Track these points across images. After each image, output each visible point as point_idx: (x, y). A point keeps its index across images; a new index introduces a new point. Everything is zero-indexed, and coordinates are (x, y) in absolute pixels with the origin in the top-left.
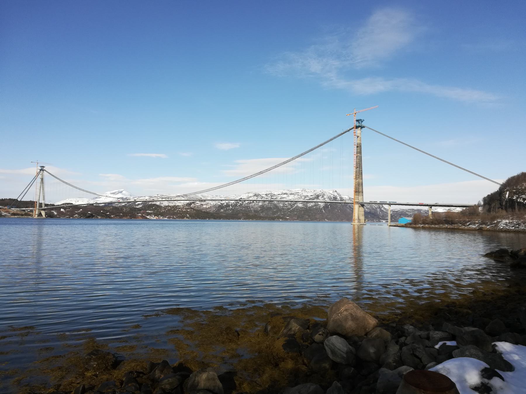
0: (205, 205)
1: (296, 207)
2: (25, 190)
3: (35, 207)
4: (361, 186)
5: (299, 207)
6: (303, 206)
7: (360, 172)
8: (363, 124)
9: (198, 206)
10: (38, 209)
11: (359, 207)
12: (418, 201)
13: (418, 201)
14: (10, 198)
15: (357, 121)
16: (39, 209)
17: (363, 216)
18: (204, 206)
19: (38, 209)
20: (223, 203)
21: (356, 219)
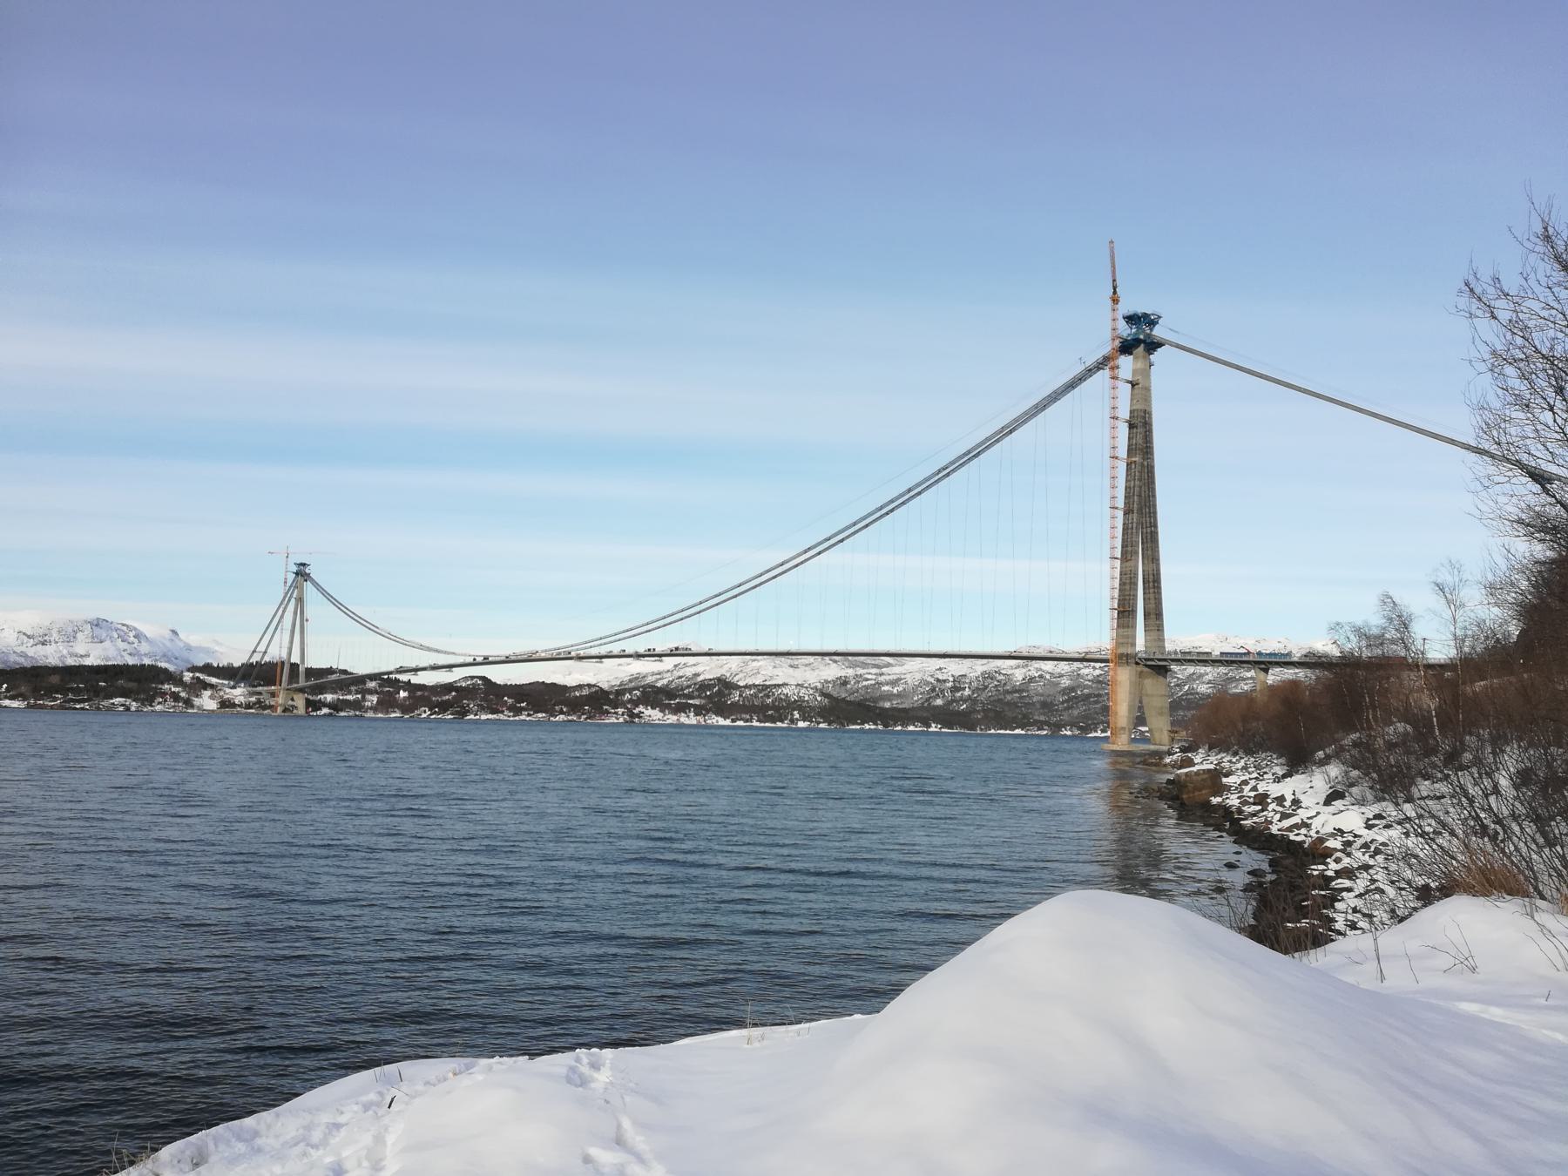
0: (887, 684)
1: (1187, 694)
2: (261, 639)
3: (278, 683)
4: (1152, 591)
5: (1198, 693)
6: (1209, 691)
7: (1149, 530)
8: (1158, 332)
9: (866, 687)
10: (284, 689)
11: (1141, 674)
12: (1057, 644)
13: (1057, 644)
14: (554, 682)
15: (1131, 319)
16: (287, 689)
17: (1161, 714)
18: (886, 688)
19: (284, 689)
20: (944, 678)
21: (1123, 728)
